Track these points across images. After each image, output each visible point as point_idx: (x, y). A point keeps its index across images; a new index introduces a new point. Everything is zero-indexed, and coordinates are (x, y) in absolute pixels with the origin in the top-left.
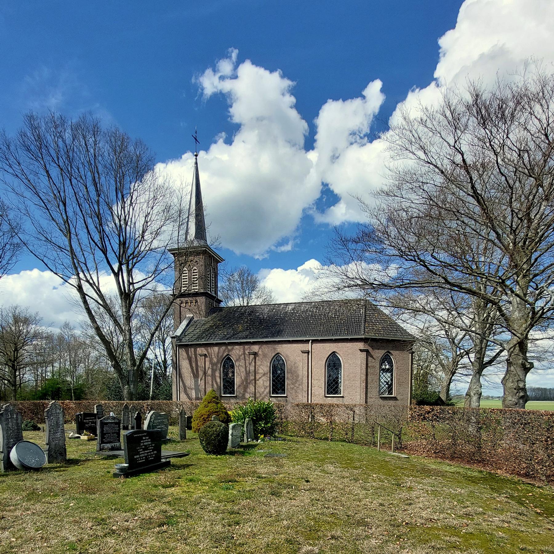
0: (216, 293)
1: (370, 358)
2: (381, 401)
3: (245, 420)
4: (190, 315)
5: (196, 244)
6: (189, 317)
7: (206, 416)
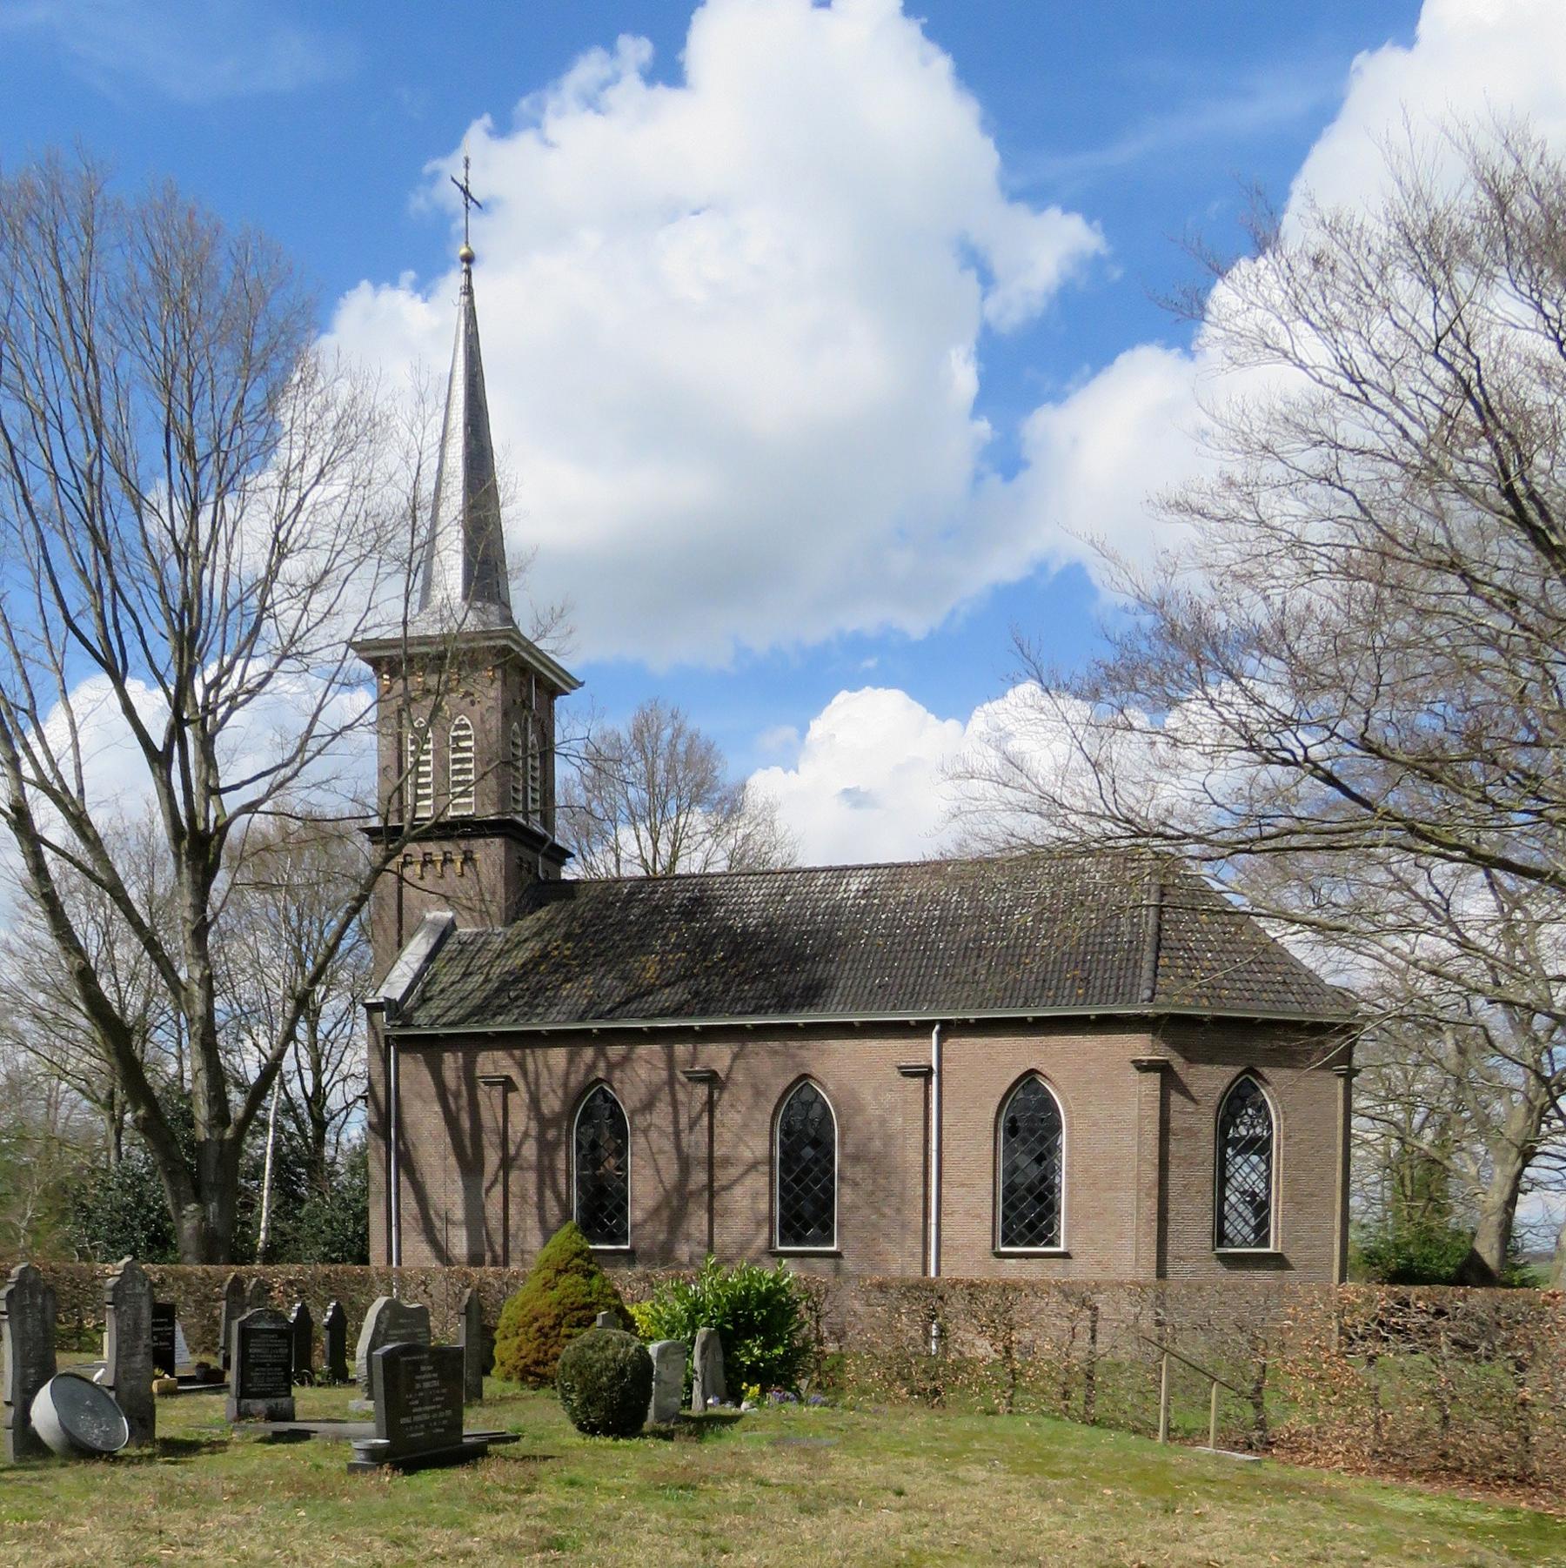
0: (548, 821)
1: (1176, 1099)
2: (1221, 1270)
3: (694, 1332)
4: (438, 914)
5: (472, 623)
6: (435, 923)
7: (549, 1322)
